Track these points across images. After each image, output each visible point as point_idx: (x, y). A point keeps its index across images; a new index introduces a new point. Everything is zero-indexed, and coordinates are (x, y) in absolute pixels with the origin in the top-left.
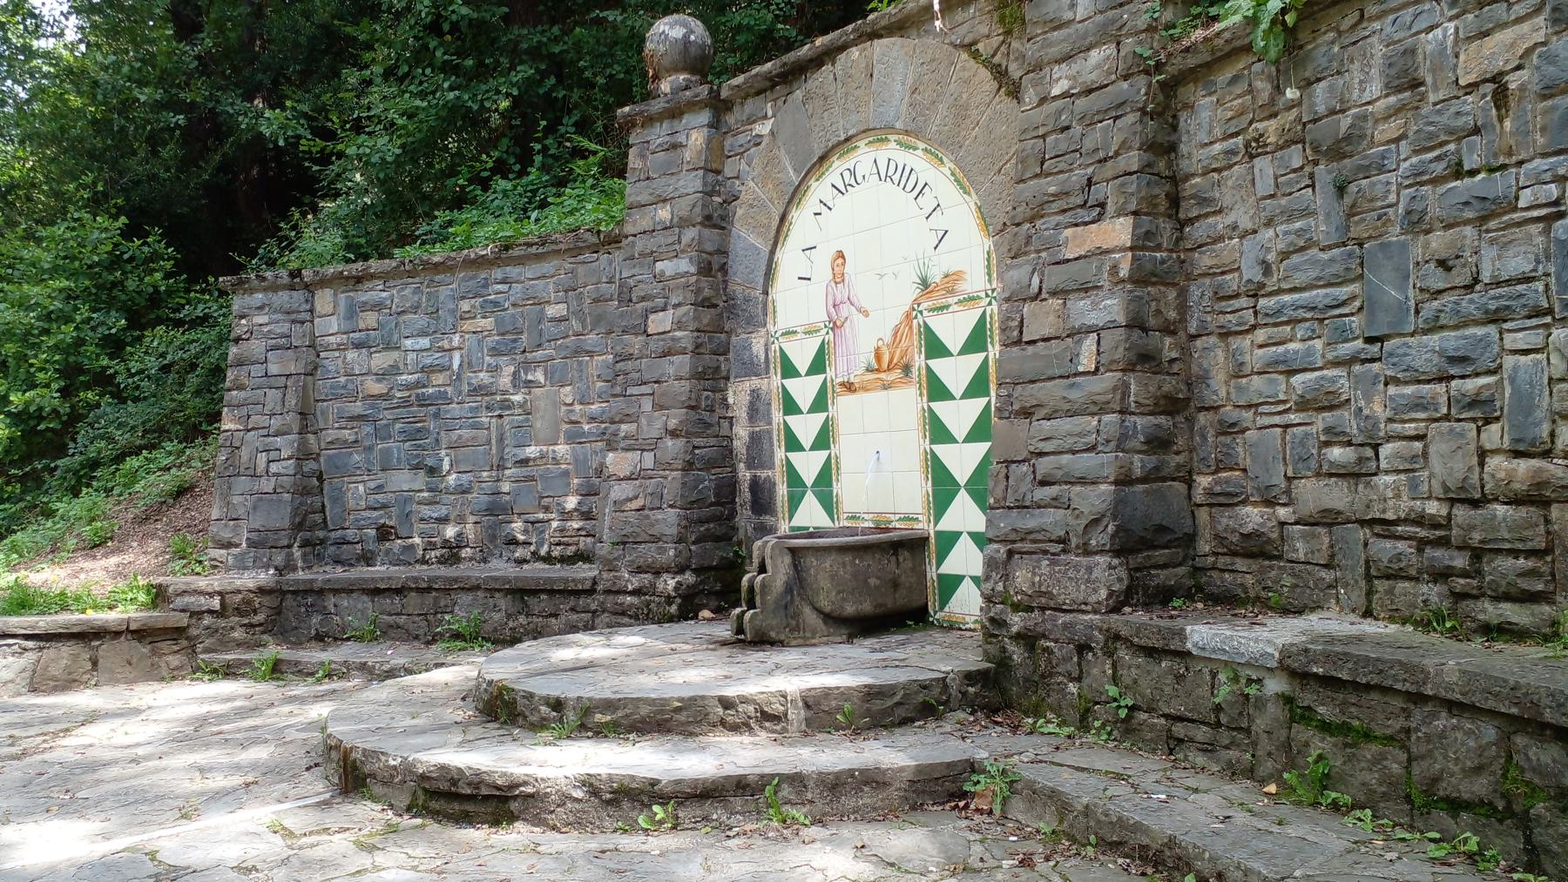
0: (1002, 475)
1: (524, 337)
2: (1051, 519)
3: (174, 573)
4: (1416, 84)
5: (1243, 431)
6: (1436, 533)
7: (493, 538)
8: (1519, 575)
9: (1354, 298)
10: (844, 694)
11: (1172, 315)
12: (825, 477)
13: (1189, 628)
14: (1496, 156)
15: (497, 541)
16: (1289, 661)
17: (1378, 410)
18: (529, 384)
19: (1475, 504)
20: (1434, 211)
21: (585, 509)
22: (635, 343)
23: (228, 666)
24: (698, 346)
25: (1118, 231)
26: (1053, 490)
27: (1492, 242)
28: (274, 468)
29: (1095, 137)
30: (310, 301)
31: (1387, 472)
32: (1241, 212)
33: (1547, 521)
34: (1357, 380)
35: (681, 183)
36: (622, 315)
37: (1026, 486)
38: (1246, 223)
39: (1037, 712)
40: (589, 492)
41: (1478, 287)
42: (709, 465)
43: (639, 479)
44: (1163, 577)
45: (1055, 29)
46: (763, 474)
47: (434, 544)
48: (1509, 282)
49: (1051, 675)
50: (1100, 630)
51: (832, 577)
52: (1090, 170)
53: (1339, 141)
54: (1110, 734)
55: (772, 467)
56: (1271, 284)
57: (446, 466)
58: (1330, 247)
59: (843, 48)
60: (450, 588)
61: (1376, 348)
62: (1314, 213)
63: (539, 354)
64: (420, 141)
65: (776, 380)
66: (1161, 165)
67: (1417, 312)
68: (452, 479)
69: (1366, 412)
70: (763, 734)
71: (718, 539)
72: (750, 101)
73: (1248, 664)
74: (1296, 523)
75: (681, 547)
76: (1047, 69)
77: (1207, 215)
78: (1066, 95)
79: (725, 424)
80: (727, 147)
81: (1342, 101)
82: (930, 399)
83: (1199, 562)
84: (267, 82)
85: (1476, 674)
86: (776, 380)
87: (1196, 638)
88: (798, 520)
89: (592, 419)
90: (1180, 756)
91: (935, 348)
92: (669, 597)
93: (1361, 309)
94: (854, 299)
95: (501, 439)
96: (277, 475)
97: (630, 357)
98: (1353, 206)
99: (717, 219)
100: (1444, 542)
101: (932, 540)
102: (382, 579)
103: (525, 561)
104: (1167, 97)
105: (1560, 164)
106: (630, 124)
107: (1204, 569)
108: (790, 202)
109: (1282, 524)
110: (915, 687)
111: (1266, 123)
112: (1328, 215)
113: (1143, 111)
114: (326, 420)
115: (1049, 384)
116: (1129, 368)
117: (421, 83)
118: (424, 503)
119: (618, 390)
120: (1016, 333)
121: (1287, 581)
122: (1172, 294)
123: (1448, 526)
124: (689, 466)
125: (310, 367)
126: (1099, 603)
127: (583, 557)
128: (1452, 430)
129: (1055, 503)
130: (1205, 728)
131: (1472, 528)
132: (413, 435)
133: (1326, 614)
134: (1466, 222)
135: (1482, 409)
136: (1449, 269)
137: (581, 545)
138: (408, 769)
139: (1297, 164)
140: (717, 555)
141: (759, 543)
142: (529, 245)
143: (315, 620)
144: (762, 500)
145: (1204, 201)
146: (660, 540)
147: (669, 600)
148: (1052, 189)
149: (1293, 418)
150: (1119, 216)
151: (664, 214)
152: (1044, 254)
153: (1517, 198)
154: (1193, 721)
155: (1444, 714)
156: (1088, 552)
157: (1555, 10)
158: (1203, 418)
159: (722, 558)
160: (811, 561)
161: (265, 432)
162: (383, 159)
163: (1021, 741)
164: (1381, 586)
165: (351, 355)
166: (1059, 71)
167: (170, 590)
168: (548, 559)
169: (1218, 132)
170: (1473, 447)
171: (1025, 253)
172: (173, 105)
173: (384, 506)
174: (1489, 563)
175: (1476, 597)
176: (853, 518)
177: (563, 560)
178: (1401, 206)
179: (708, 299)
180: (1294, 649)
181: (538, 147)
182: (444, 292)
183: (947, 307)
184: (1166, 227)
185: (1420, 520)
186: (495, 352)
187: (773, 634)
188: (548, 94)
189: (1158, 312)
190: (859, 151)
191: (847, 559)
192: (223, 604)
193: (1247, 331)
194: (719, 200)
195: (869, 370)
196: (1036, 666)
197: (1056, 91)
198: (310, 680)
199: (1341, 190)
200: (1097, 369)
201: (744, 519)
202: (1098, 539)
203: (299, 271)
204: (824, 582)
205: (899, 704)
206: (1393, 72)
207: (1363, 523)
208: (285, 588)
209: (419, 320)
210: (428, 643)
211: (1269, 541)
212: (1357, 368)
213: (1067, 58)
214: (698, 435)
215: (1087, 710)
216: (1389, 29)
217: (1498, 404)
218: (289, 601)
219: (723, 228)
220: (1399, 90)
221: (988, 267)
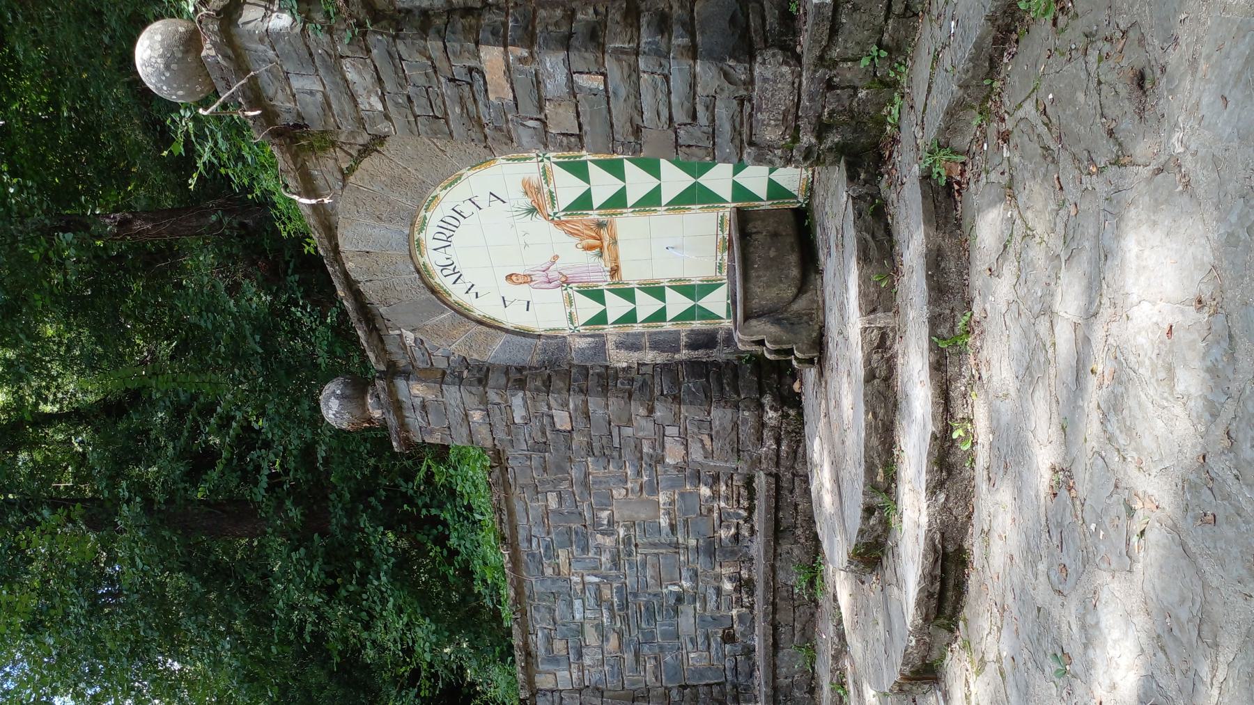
0: (687, 150)
2: (723, 111)
10: (864, 280)
12: (687, 290)
18: (611, 522)
21: (710, 480)
22: (578, 440)
24: (581, 391)
25: (491, 57)
26: (700, 109)
29: (416, 75)
30: (545, 692)
35: (452, 402)
36: (557, 450)
39: (882, 123)
40: (697, 477)
42: (676, 382)
43: (686, 439)
44: (772, 19)
45: (330, 107)
46: (684, 340)
49: (851, 111)
50: (815, 71)
51: (768, 286)
52: (442, 80)
54: (900, 64)
55: (678, 333)
57: (676, 588)
59: (346, 274)
60: (773, 587)
65: (608, 329)
68: (686, 584)
70: (896, 346)
71: (736, 377)
72: (388, 347)
76: (362, 113)
78: (382, 99)
79: (643, 369)
80: (424, 366)
82: (625, 206)
86: (608, 329)
89: (639, 474)
91: (584, 202)
92: (782, 416)
94: (545, 266)
95: (654, 545)
97: (590, 444)
99: (480, 375)
101: (739, 204)
102: (765, 640)
103: (752, 527)
104: (384, 17)
106: (407, 442)
108: (468, 317)
110: (860, 222)
114: (639, 682)
115: (614, 112)
117: (374, 602)
119: (616, 454)
120: (573, 139)
124: (677, 399)
125: (597, 694)
126: (793, 73)
127: (749, 482)
132: (651, 614)
137: (739, 484)
138: (918, 631)
140: (748, 376)
141: (739, 345)
142: (501, 521)
143: (797, 693)
144: (705, 340)
147: (785, 416)
148: (458, 110)
150: (479, 57)
151: (477, 416)
152: (510, 117)
156: (751, 81)
159: (751, 373)
160: (755, 303)
163: (905, 136)
165: (587, 661)
166: (363, 104)
168: (751, 510)
171: (509, 131)
173: (707, 638)
177: (751, 498)
181: (424, 512)
182: (538, 588)
183: (551, 193)
184: (488, 18)
186: (585, 549)
187: (814, 335)
189: (556, 24)
190: (427, 261)
194: (466, 372)
195: (601, 255)
197: (380, 107)
200: (602, 74)
201: (720, 354)
202: (741, 74)
205: (873, 236)
209: (560, 608)
210: (817, 606)
213: (353, 98)
214: (652, 392)
215: (881, 82)
219: (488, 369)
221: (519, 160)
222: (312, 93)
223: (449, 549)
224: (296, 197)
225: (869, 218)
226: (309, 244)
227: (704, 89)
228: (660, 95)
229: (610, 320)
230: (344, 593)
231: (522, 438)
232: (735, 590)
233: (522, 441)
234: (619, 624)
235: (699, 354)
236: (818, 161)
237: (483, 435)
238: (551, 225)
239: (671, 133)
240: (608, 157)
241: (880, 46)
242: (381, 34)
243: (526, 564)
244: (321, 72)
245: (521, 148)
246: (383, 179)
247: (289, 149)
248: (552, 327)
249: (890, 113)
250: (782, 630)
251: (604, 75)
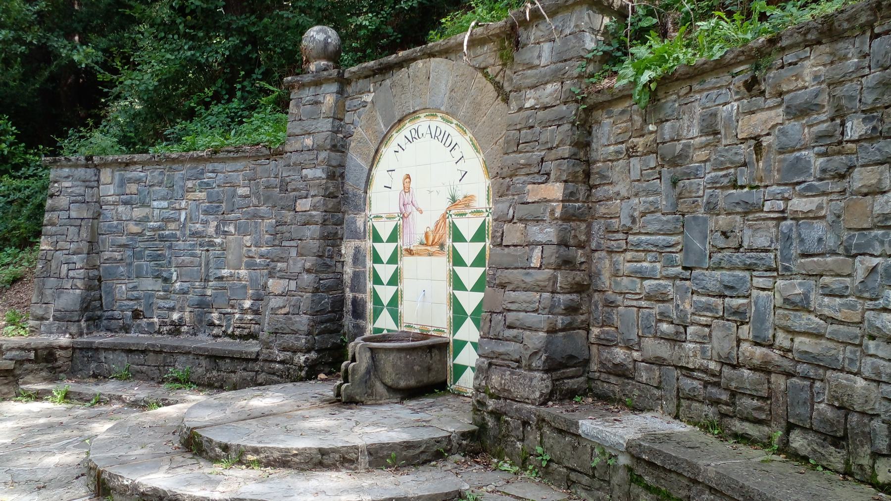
0: (488, 319)
1: (224, 205)
2: (512, 348)
3: (7, 334)
4: (716, 133)
5: (617, 306)
6: (714, 380)
7: (200, 321)
8: (754, 409)
9: (678, 244)
11: (583, 238)
12: (395, 301)
13: (580, 422)
14: (754, 180)
15: (202, 323)
16: (631, 450)
17: (687, 307)
18: (225, 233)
19: (734, 367)
20: (721, 204)
21: (255, 308)
22: (288, 215)
23: (38, 393)
25: (555, 190)
26: (514, 332)
27: (750, 226)
28: (71, 274)
29: (546, 135)
30: (98, 174)
31: (690, 342)
32: (622, 186)
33: (769, 382)
34: (678, 289)
35: (319, 125)
36: (281, 199)
37: (500, 327)
38: (624, 193)
39: (499, 456)
40: (258, 298)
41: (741, 250)
43: (287, 296)
44: (571, 383)
45: (530, 68)
46: (360, 296)
48: (757, 250)
49: (508, 436)
50: (535, 415)
51: (393, 366)
52: (543, 153)
53: (675, 157)
54: (537, 473)
55: (365, 292)
56: (636, 229)
57: (174, 277)
58: (667, 214)
59: (414, 59)
60: (174, 352)
61: (688, 273)
62: (659, 194)
64: (169, 78)
65: (369, 243)
67: (710, 257)
68: (177, 285)
69: (681, 307)
71: (331, 332)
72: (361, 81)
73: (610, 447)
74: (642, 361)
75: (309, 337)
76: (523, 92)
77: (604, 184)
78: (532, 108)
80: (347, 106)
81: (678, 135)
83: (591, 375)
84: (80, 29)
85: (724, 475)
86: (369, 243)
87: (584, 428)
88: (378, 324)
89: (262, 256)
90: (573, 490)
91: (458, 237)
92: (301, 366)
93: (681, 250)
95: (207, 264)
96: (73, 278)
97: (285, 223)
98: (680, 194)
99: (339, 147)
100: (717, 385)
101: (451, 344)
102: (134, 344)
103: (220, 337)
104: (587, 116)
105: (786, 191)
106: (291, 87)
107: (593, 379)
109: (635, 361)
110: (432, 442)
111: (638, 139)
112: (667, 196)
113: (573, 123)
114: (104, 246)
115: (516, 271)
116: (558, 268)
117: (171, 44)
118: (163, 299)
119: (277, 242)
120: (499, 240)
121: (636, 392)
122: (583, 226)
123: (719, 376)
124: (316, 290)
125: (96, 215)
126: (535, 399)
127: (253, 336)
128: (724, 325)
129: (515, 339)
130: (587, 477)
131: (732, 380)
132: (156, 258)
133: (656, 414)
134: (738, 213)
135: (740, 317)
136: (727, 237)
137: (252, 329)
138: (135, 487)
139: (653, 165)
140: (331, 341)
141: (352, 344)
143: (93, 365)
144: (358, 311)
145: (603, 177)
146: (297, 333)
147: (301, 368)
148: (522, 161)
149: (643, 303)
150: (556, 181)
151: (309, 141)
152: (516, 197)
153: (763, 206)
154: (579, 472)
155: (707, 492)
156: (530, 369)
157: (787, 107)
158: (596, 296)
159: (334, 343)
160: (382, 356)
161: (67, 252)
162: (147, 88)
163: (489, 476)
164: (684, 403)
165: (121, 208)
166: (530, 93)
167: (4, 347)
168: (232, 336)
169: (612, 139)
170: (734, 336)
171: (507, 195)
172: (19, 40)
173: (137, 299)
174: (739, 399)
175: (732, 417)
176: (409, 326)
177: (241, 337)
178: (705, 198)
179: (332, 193)
180: (634, 443)
181: (239, 86)
182: (178, 175)
183: (465, 214)
184: (582, 188)
185: (705, 371)
186: (206, 212)
187: (358, 398)
188: (247, 55)
189: (575, 236)
190: (421, 120)
191: (403, 355)
192: (36, 355)
193: (622, 252)
194: (341, 136)
195: (421, 244)
196: (501, 431)
197: (527, 105)
198: (88, 404)
199: (674, 183)
200: (541, 266)
201: (348, 321)
203: (91, 157)
204: (389, 369)
205: (422, 452)
206: (705, 124)
207: (676, 367)
208: (76, 346)
209: (162, 191)
210: (159, 383)
211: (628, 369)
212: (678, 282)
213: (534, 87)
214: (322, 272)
215: (526, 458)
216: (704, 100)
217: (748, 315)
218: (78, 354)
219: (343, 152)
220: (707, 134)
222: (539, 57)
223: (209, 103)
224: (468, 33)
226: (436, 34)
227: (527, 337)
228: (525, 305)
229: (376, 245)
230: (178, 21)
231: (291, 173)
234: (148, 234)
235: (349, 306)
236: (476, 410)
238: (443, 212)
239: (500, 309)
240: (487, 257)
241: (550, 461)
242: (576, 115)
243: (196, 168)
244: (553, 66)
245: (495, 202)
246: (479, 98)
247: (502, 32)
248: (372, 205)
249: (505, 462)
250: (142, 357)
251: (540, 268)
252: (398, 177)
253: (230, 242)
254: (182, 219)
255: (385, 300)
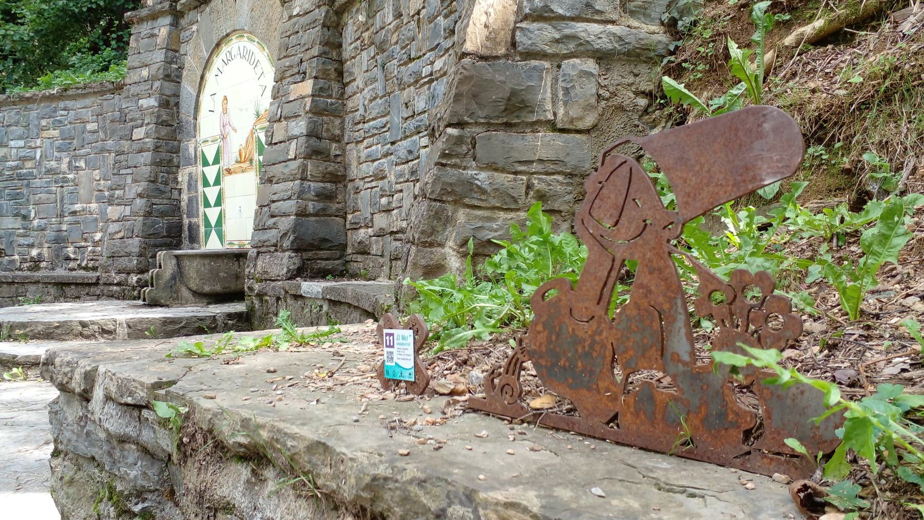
9: (387, 123)
10: (151, 321)
11: (337, 132)
18: (77, 169)
22: (126, 145)
24: (157, 147)
25: (307, 87)
42: (163, 214)
44: (323, 264)
46: (194, 220)
47: (26, 259)
49: (268, 313)
51: (197, 272)
55: (198, 216)
57: (33, 215)
63: (83, 151)
66: (334, 54)
68: (36, 222)
70: (103, 340)
75: (141, 259)
78: (298, 15)
79: (176, 193)
92: (133, 286)
95: (62, 200)
97: (123, 153)
103: (75, 270)
108: (205, 68)
116: (308, 157)
119: (116, 171)
122: (338, 122)
124: (148, 214)
132: (15, 197)
142: (78, 88)
148: (287, 64)
149: (374, 184)
151: (145, 73)
160: (186, 263)
168: (86, 268)
182: (34, 114)
184: (336, 86)
186: (60, 150)
187: (162, 301)
189: (328, 130)
191: (207, 261)
194: (176, 66)
197: (295, 13)
202: (287, 243)
205: (182, 327)
209: (18, 130)
214: (155, 197)
225: (197, 325)
232: (32, 258)
233: (129, 105)
237: (133, 77)
251: (295, 159)
252: (219, 99)
253: (82, 176)
254: (38, 157)
255: (213, 222)
